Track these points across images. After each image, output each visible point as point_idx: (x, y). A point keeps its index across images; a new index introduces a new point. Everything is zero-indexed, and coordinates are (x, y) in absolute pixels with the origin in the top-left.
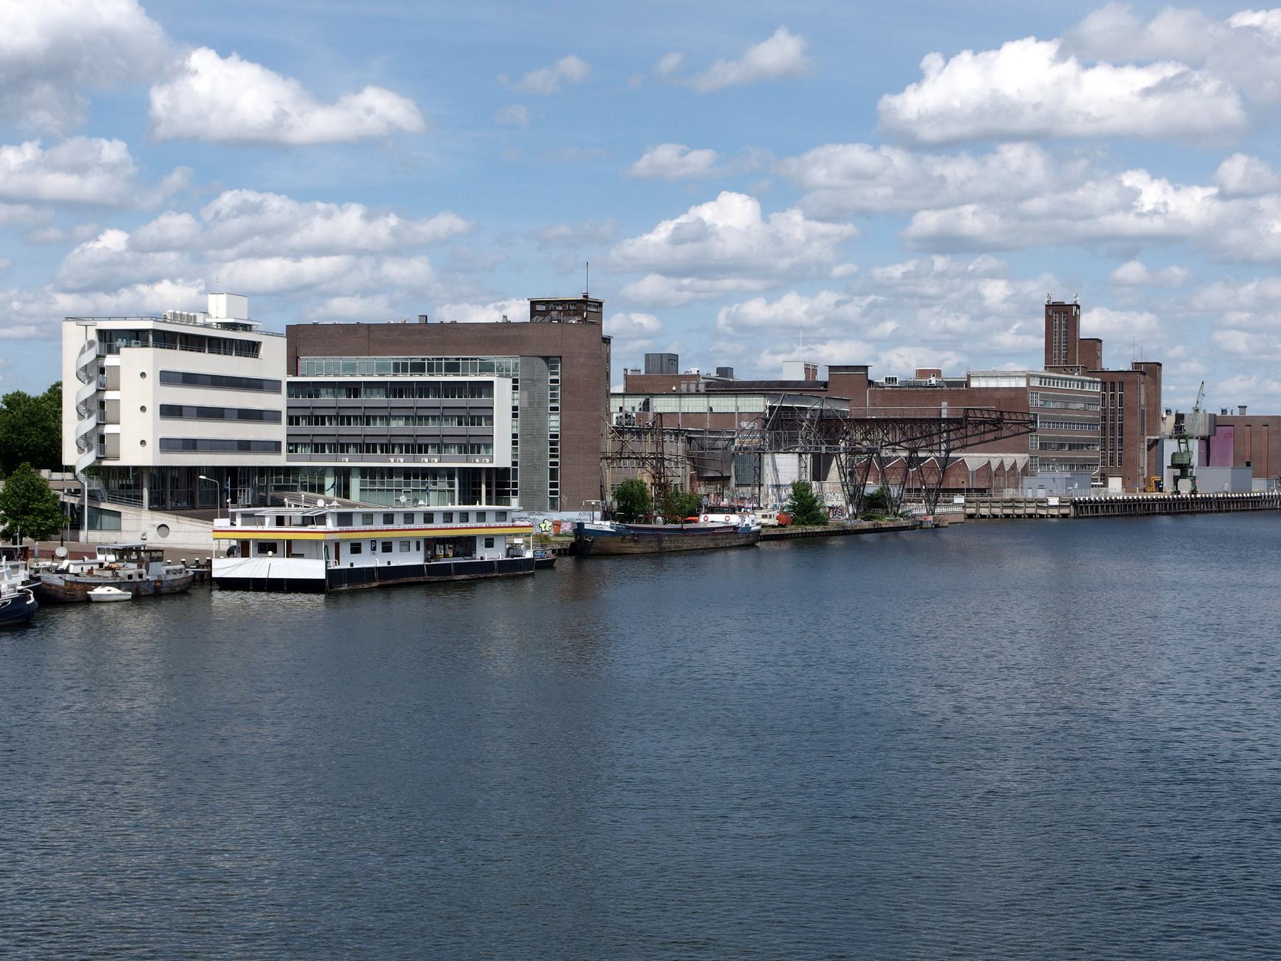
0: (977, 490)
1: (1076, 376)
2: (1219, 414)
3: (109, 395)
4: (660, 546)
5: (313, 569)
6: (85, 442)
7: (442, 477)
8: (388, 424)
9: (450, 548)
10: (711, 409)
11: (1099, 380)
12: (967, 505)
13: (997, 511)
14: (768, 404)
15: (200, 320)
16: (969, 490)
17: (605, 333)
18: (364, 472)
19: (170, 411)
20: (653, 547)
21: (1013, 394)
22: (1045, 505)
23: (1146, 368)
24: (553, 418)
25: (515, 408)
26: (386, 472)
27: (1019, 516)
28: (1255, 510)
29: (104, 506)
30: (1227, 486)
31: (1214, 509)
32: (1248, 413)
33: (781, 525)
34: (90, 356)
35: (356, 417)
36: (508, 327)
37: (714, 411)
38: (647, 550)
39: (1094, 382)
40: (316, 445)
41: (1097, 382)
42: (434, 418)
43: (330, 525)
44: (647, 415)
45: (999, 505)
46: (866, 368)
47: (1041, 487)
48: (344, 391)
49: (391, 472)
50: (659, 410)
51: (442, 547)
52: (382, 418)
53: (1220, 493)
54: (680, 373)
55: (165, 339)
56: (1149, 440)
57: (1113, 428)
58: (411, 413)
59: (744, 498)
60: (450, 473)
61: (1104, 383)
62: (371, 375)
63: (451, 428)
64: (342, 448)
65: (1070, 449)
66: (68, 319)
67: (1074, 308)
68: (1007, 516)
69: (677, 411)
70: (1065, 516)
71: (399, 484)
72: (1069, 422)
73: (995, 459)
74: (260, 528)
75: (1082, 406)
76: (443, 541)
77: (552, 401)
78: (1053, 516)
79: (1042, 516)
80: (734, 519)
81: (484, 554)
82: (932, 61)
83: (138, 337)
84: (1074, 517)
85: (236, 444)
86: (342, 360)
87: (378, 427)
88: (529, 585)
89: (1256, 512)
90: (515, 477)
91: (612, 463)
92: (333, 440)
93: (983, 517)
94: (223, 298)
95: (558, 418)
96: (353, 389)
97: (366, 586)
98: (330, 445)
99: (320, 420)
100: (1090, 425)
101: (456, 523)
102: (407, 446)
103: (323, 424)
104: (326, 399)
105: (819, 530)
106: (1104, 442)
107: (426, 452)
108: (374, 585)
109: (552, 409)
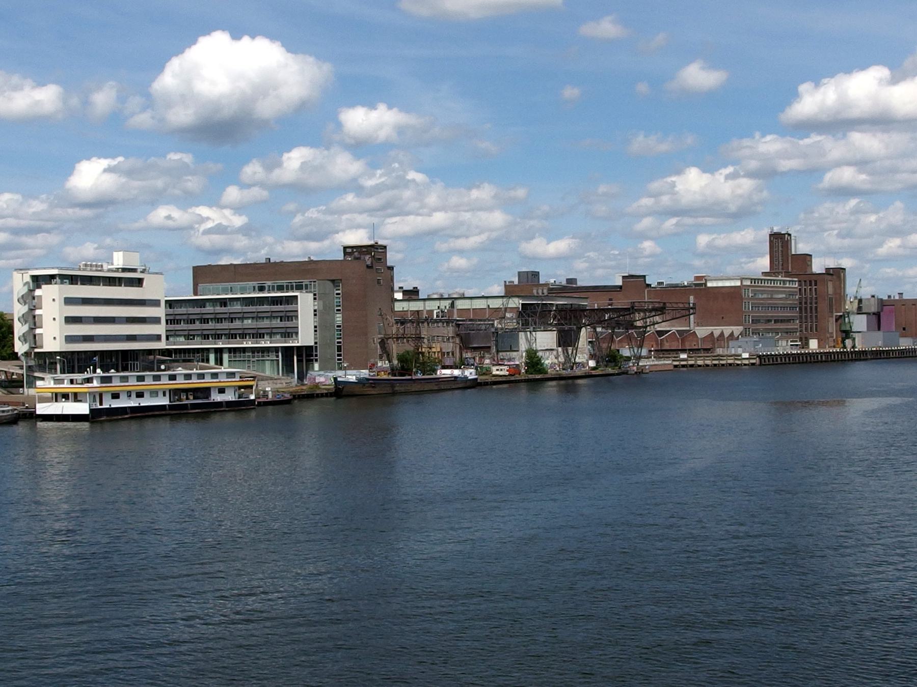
0: (705, 350)
1: (780, 278)
2: (886, 298)
3: (38, 312)
4: (393, 390)
5: (83, 408)
6: (24, 339)
7: (272, 352)
8: (243, 322)
9: (191, 395)
10: (489, 306)
11: (796, 279)
12: (689, 359)
13: (708, 362)
14: (521, 302)
15: (105, 267)
16: (690, 350)
17: (389, 264)
18: (230, 350)
19: (70, 320)
20: (389, 390)
21: (732, 290)
22: (740, 358)
23: (833, 271)
24: (338, 315)
25: (315, 311)
26: (242, 350)
27: (723, 365)
28: (901, 357)
29: (36, 374)
30: (880, 343)
31: (869, 357)
32: (905, 297)
33: (510, 375)
34: (25, 290)
35: (225, 319)
36: (311, 264)
37: (491, 307)
38: (381, 392)
39: (793, 281)
40: (205, 335)
41: (796, 281)
42: (267, 317)
43: (95, 383)
44: (453, 311)
45: (710, 358)
46: (644, 277)
47: (740, 347)
48: (218, 304)
49: (244, 350)
50: (460, 307)
51: (185, 394)
52: (239, 318)
53: (874, 347)
54: (541, 283)
55: (73, 280)
56: (836, 316)
57: (811, 308)
58: (255, 315)
59: (504, 359)
60: (276, 349)
61: (799, 281)
62: (236, 294)
63: (277, 323)
64: (218, 337)
65: (775, 322)
66: (16, 270)
67: (786, 235)
68: (715, 365)
69: (469, 307)
70: (753, 364)
71: (249, 356)
72: (774, 307)
73: (717, 330)
74: (234, 380)
75: (784, 296)
76: (186, 391)
77: (337, 306)
78: (745, 365)
79: (738, 365)
80: (457, 372)
81: (216, 397)
82: (804, 88)
83: (50, 279)
84: (759, 365)
85: (81, 337)
86: (220, 286)
87: (237, 324)
88: (253, 414)
89: (901, 359)
90: (316, 351)
91: (397, 340)
92: (213, 332)
93: (700, 366)
94: (121, 253)
95: (341, 315)
96: (224, 302)
97: (120, 417)
98: (212, 335)
99: (206, 321)
100: (790, 307)
101: (194, 380)
102: (253, 334)
103: (208, 323)
104: (209, 309)
105: (539, 377)
106: (801, 317)
107: (263, 338)
108: (126, 416)
109: (338, 310)
